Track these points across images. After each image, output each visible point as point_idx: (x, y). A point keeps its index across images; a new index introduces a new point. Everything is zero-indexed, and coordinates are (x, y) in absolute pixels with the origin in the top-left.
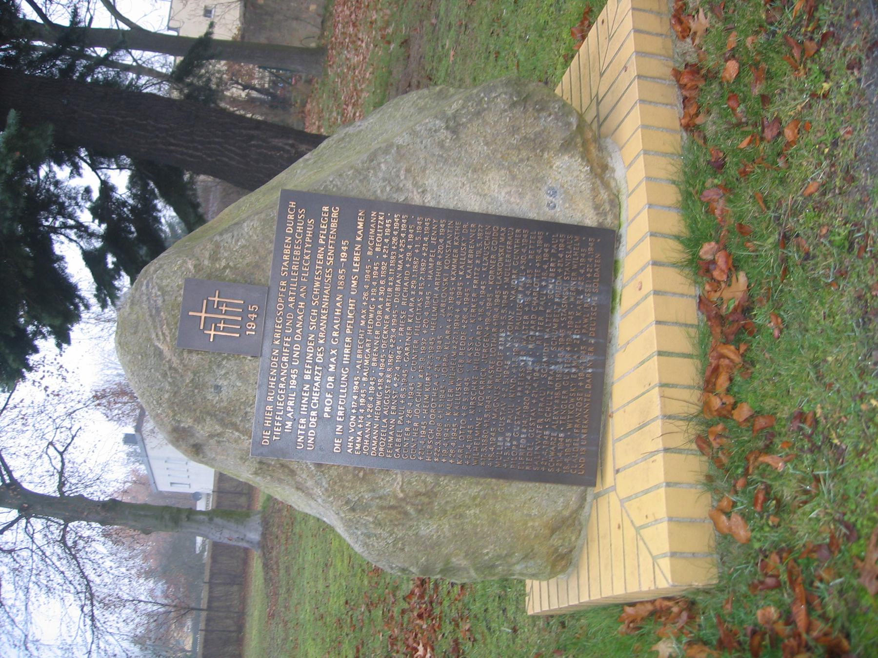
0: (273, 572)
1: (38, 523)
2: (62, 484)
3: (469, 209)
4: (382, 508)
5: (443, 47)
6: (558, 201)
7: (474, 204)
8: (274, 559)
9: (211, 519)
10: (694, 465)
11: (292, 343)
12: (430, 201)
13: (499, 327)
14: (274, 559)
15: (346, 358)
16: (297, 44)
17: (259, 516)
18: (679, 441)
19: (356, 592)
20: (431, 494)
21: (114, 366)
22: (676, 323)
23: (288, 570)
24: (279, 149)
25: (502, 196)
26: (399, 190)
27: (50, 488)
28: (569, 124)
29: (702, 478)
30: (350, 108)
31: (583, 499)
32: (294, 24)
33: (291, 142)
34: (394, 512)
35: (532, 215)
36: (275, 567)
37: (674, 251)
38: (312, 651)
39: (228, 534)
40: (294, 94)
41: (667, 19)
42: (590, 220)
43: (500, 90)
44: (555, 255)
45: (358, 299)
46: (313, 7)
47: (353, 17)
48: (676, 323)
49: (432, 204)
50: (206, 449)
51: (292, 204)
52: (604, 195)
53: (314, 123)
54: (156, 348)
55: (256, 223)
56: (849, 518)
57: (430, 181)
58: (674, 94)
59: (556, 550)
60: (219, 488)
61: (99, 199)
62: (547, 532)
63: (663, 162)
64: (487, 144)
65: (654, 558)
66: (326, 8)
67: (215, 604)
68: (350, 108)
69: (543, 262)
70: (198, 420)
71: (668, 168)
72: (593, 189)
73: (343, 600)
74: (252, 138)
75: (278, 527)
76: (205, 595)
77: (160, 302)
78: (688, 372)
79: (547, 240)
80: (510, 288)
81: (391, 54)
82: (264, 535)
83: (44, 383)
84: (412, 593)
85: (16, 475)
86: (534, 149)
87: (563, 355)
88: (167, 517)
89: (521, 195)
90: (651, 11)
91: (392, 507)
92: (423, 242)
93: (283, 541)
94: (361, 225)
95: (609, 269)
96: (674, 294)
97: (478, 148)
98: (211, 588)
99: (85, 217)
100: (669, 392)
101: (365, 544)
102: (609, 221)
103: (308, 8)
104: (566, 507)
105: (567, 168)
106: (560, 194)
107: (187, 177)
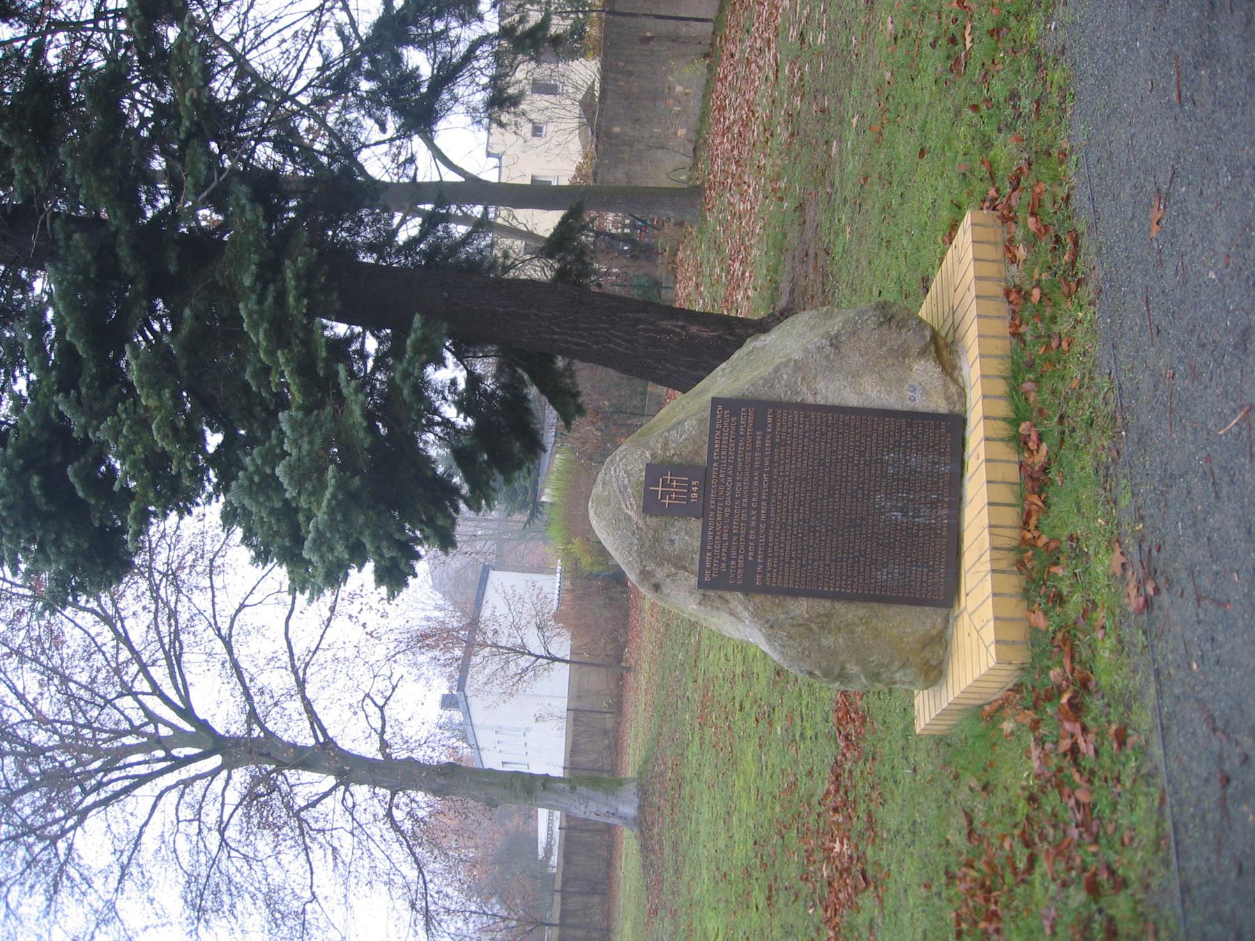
0: (655, 854)
1: (361, 792)
2: (384, 745)
3: (850, 405)
4: (793, 626)
5: (839, 221)
6: (918, 395)
7: (853, 400)
8: (656, 838)
9: (573, 788)
10: (1013, 582)
11: (724, 507)
12: (820, 400)
13: (875, 491)
14: (656, 838)
15: (763, 516)
16: (666, 183)
17: (635, 784)
18: (1003, 565)
19: (766, 824)
20: (829, 615)
21: (421, 605)
22: (1003, 482)
23: (675, 846)
24: (669, 332)
25: (874, 394)
26: (797, 393)
27: (370, 750)
28: (924, 336)
29: (1021, 591)
30: (737, 264)
31: (946, 621)
32: (659, 154)
33: (680, 323)
34: (801, 629)
35: (898, 407)
36: (657, 847)
37: (1002, 429)
38: (713, 923)
39: (592, 808)
40: (661, 240)
41: (1001, 249)
42: (943, 408)
43: (870, 313)
44: (916, 436)
45: (770, 473)
46: (682, 132)
47: (736, 152)
48: (1003, 482)
49: (822, 402)
50: (664, 588)
51: (720, 407)
52: (953, 389)
53: (691, 279)
54: (626, 514)
55: (694, 422)
56: (1092, 597)
57: (821, 386)
58: (1004, 308)
59: (928, 661)
60: (572, 763)
61: (466, 390)
62: (919, 646)
63: (994, 362)
64: (861, 356)
65: (987, 648)
66: (698, 132)
67: (570, 921)
68: (737, 264)
69: (906, 442)
70: (659, 565)
71: (997, 367)
72: (944, 385)
73: (750, 843)
74: (639, 321)
75: (660, 796)
76: (557, 909)
77: (626, 482)
78: (1010, 516)
79: (909, 425)
80: (882, 462)
81: (784, 213)
82: (641, 808)
83: (362, 620)
84: (828, 793)
85: (331, 734)
86: (898, 358)
87: (924, 510)
88: (518, 785)
89: (889, 393)
90: (988, 242)
91: (801, 625)
92: (815, 430)
93: (667, 811)
94: (770, 420)
95: (960, 443)
96: (1002, 461)
97: (856, 359)
98: (563, 899)
99: (450, 412)
100: (995, 531)
101: (782, 653)
102: (957, 409)
103: (676, 133)
104: (934, 627)
105: (924, 371)
106: (920, 389)
107: (560, 363)
